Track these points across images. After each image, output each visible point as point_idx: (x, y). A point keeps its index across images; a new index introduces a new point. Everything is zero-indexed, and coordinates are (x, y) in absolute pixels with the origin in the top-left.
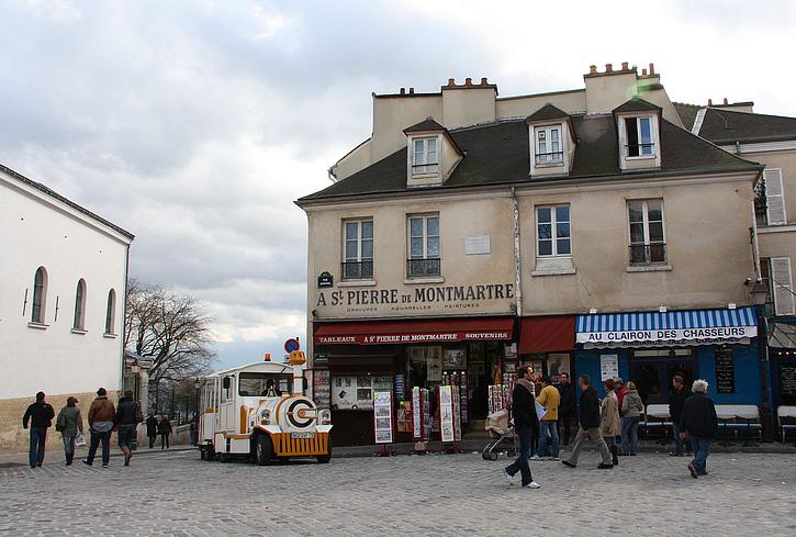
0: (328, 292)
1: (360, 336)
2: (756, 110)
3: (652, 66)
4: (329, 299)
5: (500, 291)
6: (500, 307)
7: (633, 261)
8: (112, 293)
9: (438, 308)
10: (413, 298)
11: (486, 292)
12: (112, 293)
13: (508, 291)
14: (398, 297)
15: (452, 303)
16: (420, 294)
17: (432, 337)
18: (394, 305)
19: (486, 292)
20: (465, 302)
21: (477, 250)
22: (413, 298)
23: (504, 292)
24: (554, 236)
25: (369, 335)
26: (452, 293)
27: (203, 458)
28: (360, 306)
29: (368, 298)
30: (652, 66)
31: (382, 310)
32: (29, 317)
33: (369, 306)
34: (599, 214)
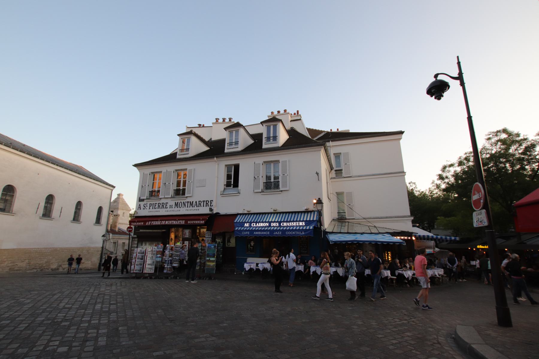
0: (142, 203)
1: (145, 222)
2: (350, 131)
3: (298, 112)
4: (142, 207)
5: (207, 203)
6: (205, 210)
7: (267, 189)
8: (100, 209)
9: (183, 211)
10: (174, 206)
11: (202, 204)
12: (100, 209)
13: (211, 203)
14: (168, 206)
15: (189, 208)
16: (176, 205)
17: (163, 223)
18: (166, 209)
19: (202, 204)
20: (193, 208)
21: (207, 189)
22: (174, 206)
23: (209, 204)
24: (233, 180)
25: (148, 221)
26: (189, 204)
27: (276, 291)
28: (154, 210)
29: (157, 206)
30: (298, 112)
31: (162, 212)
32: (41, 211)
33: (157, 210)
34: (250, 168)
